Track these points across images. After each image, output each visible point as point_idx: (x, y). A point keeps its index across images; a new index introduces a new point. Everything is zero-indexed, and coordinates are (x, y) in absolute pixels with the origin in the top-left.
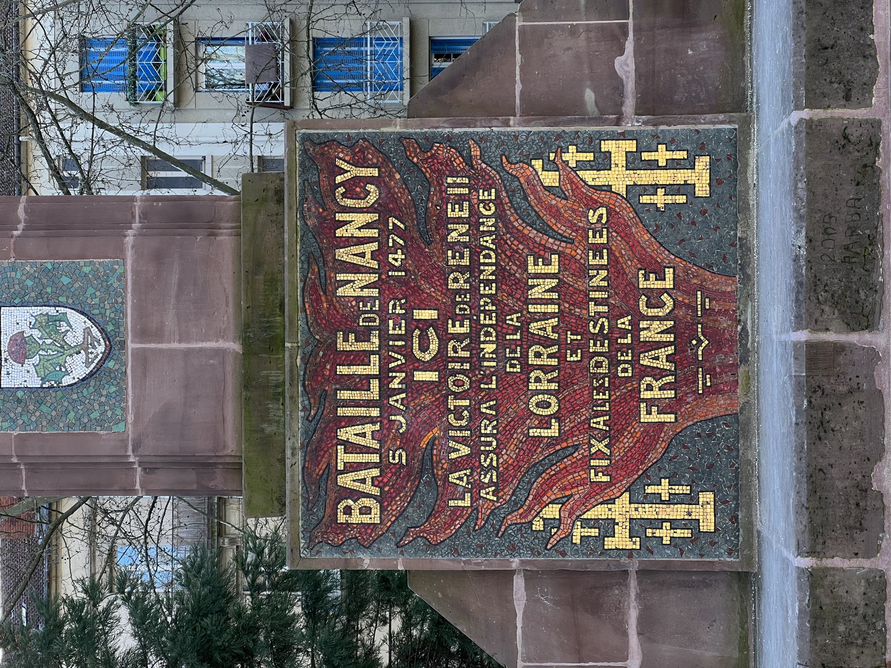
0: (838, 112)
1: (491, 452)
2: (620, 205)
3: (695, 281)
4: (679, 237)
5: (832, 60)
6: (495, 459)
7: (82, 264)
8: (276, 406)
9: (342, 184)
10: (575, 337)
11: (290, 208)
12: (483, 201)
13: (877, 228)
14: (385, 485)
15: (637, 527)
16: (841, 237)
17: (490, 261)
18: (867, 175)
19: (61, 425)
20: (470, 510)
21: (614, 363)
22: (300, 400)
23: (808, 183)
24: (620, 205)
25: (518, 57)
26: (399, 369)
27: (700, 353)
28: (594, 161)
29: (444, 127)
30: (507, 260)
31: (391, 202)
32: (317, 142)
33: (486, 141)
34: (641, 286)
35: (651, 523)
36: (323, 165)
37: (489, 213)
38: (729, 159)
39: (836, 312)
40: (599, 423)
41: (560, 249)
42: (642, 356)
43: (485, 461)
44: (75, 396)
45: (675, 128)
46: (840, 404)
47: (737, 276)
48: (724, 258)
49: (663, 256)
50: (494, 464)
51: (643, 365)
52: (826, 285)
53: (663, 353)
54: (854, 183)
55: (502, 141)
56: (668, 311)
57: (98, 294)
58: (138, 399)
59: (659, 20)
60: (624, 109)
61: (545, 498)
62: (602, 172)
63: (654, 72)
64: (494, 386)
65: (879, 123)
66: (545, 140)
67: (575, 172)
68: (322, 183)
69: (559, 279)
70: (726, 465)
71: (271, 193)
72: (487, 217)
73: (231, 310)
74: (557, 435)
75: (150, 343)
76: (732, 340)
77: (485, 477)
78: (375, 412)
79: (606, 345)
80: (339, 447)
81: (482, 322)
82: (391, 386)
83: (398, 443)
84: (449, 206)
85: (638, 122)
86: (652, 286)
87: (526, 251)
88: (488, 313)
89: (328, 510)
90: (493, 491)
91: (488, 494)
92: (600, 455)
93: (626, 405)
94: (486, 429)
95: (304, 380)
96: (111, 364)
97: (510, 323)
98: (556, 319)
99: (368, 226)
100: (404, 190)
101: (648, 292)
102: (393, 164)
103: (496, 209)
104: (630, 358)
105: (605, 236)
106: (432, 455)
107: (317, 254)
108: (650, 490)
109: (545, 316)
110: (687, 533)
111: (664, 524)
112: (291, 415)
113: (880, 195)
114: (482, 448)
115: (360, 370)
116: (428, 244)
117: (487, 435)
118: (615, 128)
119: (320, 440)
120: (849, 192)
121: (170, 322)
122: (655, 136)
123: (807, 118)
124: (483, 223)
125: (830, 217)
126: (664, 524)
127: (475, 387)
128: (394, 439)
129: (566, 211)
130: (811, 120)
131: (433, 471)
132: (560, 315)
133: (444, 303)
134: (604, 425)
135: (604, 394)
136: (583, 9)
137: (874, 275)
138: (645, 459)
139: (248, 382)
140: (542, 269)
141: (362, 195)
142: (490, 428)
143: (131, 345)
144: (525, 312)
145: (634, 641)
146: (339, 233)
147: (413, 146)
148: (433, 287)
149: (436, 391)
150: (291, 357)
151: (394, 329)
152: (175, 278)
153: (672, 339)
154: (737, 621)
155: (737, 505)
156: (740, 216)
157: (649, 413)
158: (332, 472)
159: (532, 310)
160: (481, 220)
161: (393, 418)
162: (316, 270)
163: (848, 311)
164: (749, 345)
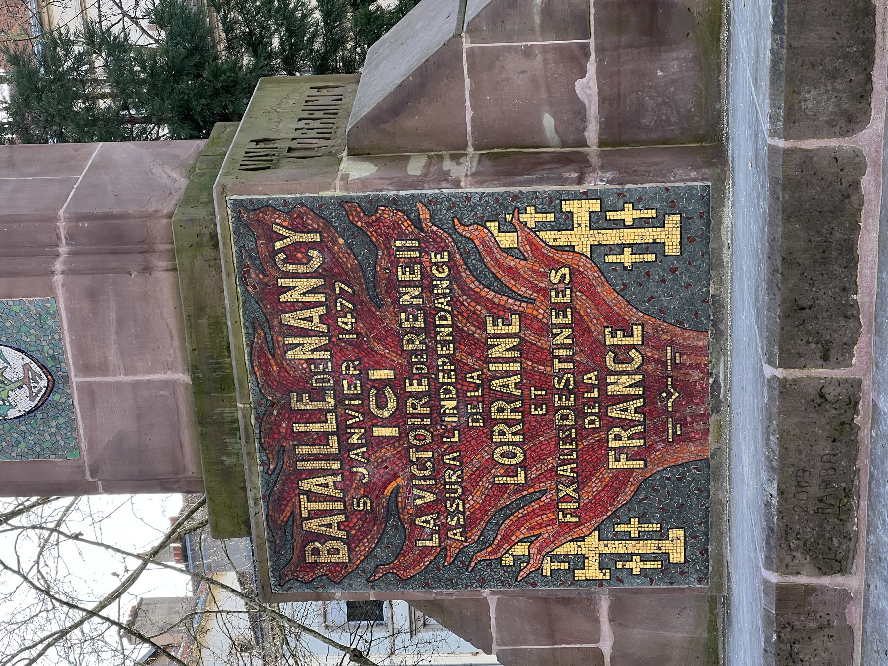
0: (814, 372)
1: (457, 498)
2: (584, 265)
3: (665, 337)
4: (648, 295)
5: (821, 61)
6: (461, 503)
7: (11, 303)
8: (233, 440)
9: (281, 250)
10: (539, 393)
11: (228, 275)
12: (435, 264)
13: (853, 481)
14: (352, 529)
15: (605, 561)
16: (815, 490)
17: (446, 322)
18: (844, 432)
19: (14, 454)
20: (438, 549)
21: (580, 415)
22: (258, 456)
23: (781, 439)
24: (584, 265)
25: (467, 81)
26: (358, 425)
27: (670, 404)
28: (554, 221)
29: (388, 190)
30: (464, 321)
31: (337, 267)
32: (251, 208)
33: (435, 204)
34: (608, 343)
35: (621, 557)
36: (260, 232)
37: (443, 275)
38: (701, 217)
39: (808, 557)
40: (567, 470)
41: (521, 309)
42: (609, 408)
43: (451, 506)
44: (23, 428)
45: (643, 186)
46: (809, 638)
47: (710, 332)
48: (696, 315)
49: (633, 315)
50: (461, 508)
51: (611, 417)
52: (798, 533)
53: (632, 405)
54: (830, 440)
55: (453, 203)
56: (636, 366)
57: (32, 331)
58: (90, 430)
59: (625, 39)
60: (586, 134)
61: (513, 538)
62: (564, 233)
63: (619, 95)
64: (457, 440)
65: (860, 382)
66: (501, 201)
67: (535, 232)
68: (260, 249)
69: (520, 338)
70: (697, 505)
71: (206, 238)
72: (441, 279)
73: (176, 343)
74: (523, 482)
75: (94, 376)
76: (704, 393)
77: (452, 520)
78: (336, 466)
79: (572, 399)
80: (302, 497)
81: (440, 381)
82: (351, 441)
83: (362, 492)
84: (399, 269)
85: (602, 181)
86: (620, 343)
87: (484, 312)
88: (447, 372)
89: (296, 552)
90: (461, 533)
91: (456, 535)
92: (567, 499)
93: (592, 458)
94: (450, 478)
95: (260, 437)
96: (56, 397)
97: (471, 380)
98: (519, 377)
99: (314, 291)
100: (349, 254)
101: (615, 349)
102: (335, 228)
103: (450, 271)
104: (597, 411)
105: (568, 296)
106: (397, 501)
107: (262, 319)
108: (618, 528)
109: (507, 374)
110: (657, 565)
111: (634, 557)
112: (250, 470)
113: (857, 451)
114: (448, 495)
115: (317, 427)
116: (379, 307)
117: (451, 484)
118: (576, 188)
119: (282, 491)
120: (824, 448)
121: (113, 357)
122: (620, 195)
123: (781, 377)
124: (437, 285)
125: (804, 471)
126: (634, 557)
127: (437, 440)
128: (358, 488)
129: (525, 272)
130: (785, 380)
131: (399, 516)
132: (522, 372)
133: (400, 364)
134: (572, 471)
135: (571, 444)
136: (538, 29)
137: (849, 525)
138: (614, 501)
139: (202, 419)
140: (501, 329)
141: (305, 261)
142: (454, 477)
143: (75, 380)
144: (485, 371)
145: (606, 626)
146: (283, 298)
147: (356, 210)
148: (387, 349)
149: (397, 444)
150: (244, 417)
151: (349, 389)
152: (113, 316)
153: (641, 393)
154: (707, 609)
155: (707, 540)
156: (712, 273)
157: (618, 460)
158: (296, 518)
159: (494, 369)
160: (434, 283)
161: (355, 470)
162: (263, 335)
163: (820, 557)
164: (721, 396)
